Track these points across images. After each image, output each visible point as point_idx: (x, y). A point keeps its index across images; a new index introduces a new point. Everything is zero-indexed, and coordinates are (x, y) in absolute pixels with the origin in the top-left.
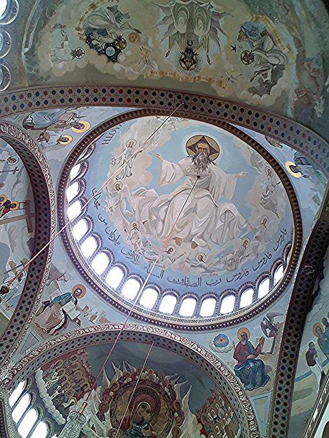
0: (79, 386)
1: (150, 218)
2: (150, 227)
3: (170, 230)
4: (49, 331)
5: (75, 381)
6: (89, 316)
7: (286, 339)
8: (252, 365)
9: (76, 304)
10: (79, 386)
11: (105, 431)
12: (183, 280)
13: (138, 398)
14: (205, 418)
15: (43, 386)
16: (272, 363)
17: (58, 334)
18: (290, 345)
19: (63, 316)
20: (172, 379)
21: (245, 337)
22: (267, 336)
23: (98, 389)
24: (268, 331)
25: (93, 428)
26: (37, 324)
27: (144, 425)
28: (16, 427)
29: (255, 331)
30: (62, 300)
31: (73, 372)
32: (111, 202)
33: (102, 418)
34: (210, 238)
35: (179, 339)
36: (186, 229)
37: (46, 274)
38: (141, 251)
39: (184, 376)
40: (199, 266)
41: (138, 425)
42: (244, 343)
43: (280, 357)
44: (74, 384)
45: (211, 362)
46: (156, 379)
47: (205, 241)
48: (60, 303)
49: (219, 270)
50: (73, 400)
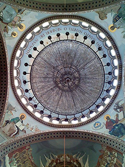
4: (10, 136)
8: (117, 127)
9: (22, 123)
17: (15, 137)
19: (17, 128)
20: (77, 156)
21: (108, 118)
22: (119, 112)
24: (118, 110)
26: (3, 131)
30: (15, 121)
31: (25, 162)
37: (6, 107)
42: (109, 121)
46: (68, 159)
48: (14, 122)
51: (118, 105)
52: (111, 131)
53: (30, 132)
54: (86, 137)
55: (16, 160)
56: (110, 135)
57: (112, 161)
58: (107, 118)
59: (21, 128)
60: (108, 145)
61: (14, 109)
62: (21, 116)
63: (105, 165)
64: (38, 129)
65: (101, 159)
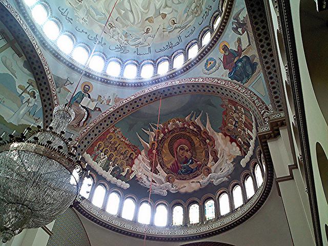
0: (127, 157)
1: (120, 13)
2: (124, 21)
3: (140, 16)
4: (79, 125)
5: (122, 154)
6: (105, 102)
7: (255, 30)
8: (240, 64)
9: (89, 97)
10: (127, 157)
11: (163, 180)
12: (167, 46)
13: (176, 145)
14: (228, 130)
15: (98, 167)
16: (253, 53)
17: (87, 124)
18: (259, 20)
19: (85, 110)
20: (191, 117)
21: (225, 48)
22: (241, 35)
23: (143, 153)
24: (240, 30)
25: (153, 181)
27: (189, 161)
28: (89, 201)
29: (231, 39)
31: (116, 148)
32: (81, 14)
33: (156, 172)
34: (173, 3)
35: (179, 82)
36: (152, 7)
38: (126, 42)
39: (198, 109)
40: (174, 29)
41: (184, 164)
42: (227, 54)
43: (257, 45)
44: (122, 156)
45: (209, 82)
46: (180, 124)
47: (170, 7)
49: (190, 21)
50: (128, 168)
51: (237, 20)
52: (232, 72)
53: (108, 109)
54: (195, 90)
55: (101, 152)
56: (230, 79)
57: (240, 119)
58: (224, 48)
59: (91, 107)
60: (229, 97)
61: (68, 82)
62: (85, 86)
63: (232, 124)
64: (119, 98)
65: (226, 116)
